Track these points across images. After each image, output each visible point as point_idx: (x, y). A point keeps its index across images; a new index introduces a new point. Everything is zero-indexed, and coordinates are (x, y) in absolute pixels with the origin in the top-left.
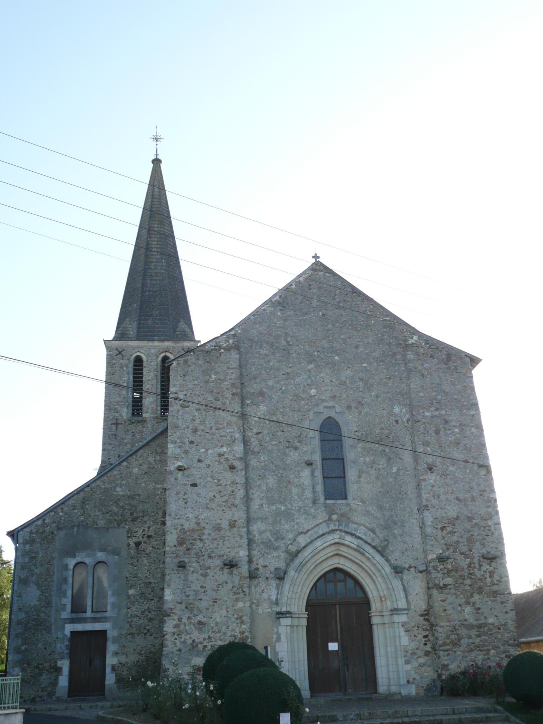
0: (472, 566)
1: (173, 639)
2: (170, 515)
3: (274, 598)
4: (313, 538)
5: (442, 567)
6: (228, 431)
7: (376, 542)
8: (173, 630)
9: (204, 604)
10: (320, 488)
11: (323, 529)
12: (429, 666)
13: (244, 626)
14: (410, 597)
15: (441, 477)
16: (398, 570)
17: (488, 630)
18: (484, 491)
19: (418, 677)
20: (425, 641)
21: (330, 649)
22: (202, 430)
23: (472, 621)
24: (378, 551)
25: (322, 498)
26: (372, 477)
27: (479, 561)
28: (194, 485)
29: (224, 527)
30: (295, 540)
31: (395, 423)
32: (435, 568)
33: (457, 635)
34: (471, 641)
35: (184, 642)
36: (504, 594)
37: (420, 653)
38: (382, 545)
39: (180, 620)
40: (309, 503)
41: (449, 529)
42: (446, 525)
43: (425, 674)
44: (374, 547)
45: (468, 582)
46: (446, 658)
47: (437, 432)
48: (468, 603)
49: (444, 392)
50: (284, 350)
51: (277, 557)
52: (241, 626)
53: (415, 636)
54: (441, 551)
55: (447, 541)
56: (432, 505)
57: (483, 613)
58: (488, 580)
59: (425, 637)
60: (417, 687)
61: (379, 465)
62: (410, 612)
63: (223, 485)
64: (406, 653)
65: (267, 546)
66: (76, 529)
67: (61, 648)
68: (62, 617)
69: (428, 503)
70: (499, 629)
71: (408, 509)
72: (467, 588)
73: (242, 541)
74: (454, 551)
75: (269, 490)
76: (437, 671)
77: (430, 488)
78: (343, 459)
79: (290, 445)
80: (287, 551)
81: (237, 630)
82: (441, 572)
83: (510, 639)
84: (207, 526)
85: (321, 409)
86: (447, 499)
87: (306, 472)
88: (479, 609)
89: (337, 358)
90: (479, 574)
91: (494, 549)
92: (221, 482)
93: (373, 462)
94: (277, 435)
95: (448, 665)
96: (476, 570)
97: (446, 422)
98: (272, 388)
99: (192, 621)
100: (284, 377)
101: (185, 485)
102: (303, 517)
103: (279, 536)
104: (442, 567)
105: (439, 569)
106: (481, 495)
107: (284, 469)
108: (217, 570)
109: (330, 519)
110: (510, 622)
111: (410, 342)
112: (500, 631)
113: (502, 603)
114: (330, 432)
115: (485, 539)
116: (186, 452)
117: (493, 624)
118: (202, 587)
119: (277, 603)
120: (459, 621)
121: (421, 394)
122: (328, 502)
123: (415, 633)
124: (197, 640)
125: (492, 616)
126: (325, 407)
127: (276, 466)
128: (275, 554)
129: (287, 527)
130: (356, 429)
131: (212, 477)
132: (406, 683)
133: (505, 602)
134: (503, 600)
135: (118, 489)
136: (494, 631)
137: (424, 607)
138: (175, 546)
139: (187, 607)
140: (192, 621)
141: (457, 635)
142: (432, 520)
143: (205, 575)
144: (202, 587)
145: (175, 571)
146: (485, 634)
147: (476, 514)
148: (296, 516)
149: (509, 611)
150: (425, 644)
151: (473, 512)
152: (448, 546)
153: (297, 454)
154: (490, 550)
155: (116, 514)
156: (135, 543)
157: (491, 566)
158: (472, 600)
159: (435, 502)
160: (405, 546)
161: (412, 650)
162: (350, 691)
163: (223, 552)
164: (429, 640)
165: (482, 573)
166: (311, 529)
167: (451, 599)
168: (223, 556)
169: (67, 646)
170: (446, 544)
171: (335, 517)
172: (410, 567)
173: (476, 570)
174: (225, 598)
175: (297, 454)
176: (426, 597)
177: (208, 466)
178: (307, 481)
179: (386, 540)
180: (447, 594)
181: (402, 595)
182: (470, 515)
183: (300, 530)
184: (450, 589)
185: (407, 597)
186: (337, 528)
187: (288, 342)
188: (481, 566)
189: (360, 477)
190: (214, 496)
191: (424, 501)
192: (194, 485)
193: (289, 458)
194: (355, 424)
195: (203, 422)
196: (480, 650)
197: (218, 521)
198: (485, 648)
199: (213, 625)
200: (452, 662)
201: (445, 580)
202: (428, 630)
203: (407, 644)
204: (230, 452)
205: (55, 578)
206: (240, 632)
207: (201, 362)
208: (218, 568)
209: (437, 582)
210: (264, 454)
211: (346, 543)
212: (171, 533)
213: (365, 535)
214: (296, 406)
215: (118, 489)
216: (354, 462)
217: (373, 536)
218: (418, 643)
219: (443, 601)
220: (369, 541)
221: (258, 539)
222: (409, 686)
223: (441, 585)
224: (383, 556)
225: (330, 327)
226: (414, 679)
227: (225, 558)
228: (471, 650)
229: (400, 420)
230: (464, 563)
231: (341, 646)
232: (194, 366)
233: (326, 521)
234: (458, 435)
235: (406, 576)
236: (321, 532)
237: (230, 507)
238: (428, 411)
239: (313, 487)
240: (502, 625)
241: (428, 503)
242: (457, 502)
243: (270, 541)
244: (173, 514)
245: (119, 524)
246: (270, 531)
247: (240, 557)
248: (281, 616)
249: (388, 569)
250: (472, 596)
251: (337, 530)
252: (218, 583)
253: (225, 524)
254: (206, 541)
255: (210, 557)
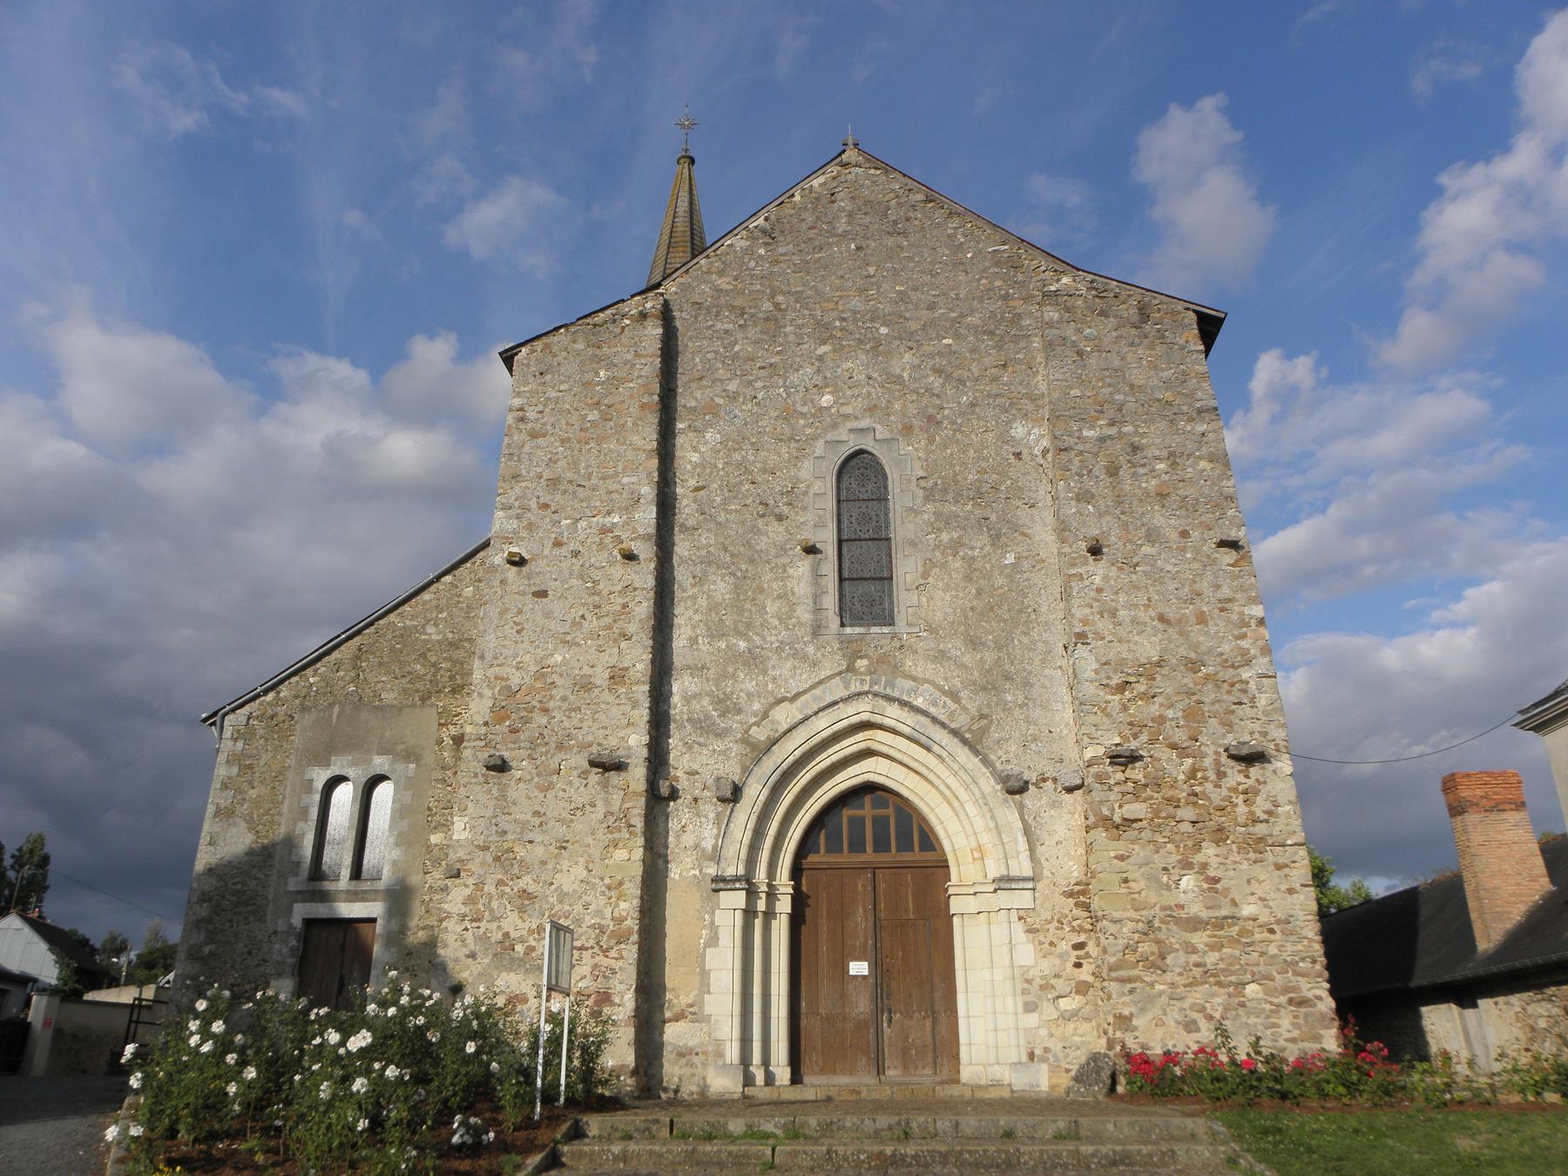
0: (1199, 775)
1: (459, 929)
2: (482, 657)
3: (708, 844)
4: (810, 712)
5: (1120, 776)
6: (626, 480)
7: (961, 721)
8: (464, 909)
9: (539, 852)
10: (830, 601)
11: (836, 690)
12: (1088, 1020)
13: (623, 905)
14: (1039, 850)
15: (1120, 569)
16: (1016, 788)
17: (1241, 934)
18: (1230, 600)
19: (1056, 1047)
20: (1078, 957)
21: (852, 972)
22: (570, 482)
23: (1196, 909)
24: (964, 741)
25: (834, 622)
26: (954, 575)
27: (1217, 763)
28: (542, 594)
29: (598, 683)
30: (765, 715)
31: (1012, 460)
32: (1101, 779)
33: (1158, 942)
34: (1194, 958)
35: (484, 939)
36: (1283, 845)
37: (1061, 986)
38: (975, 727)
39: (479, 886)
40: (804, 633)
41: (1142, 688)
42: (1132, 679)
43: (1076, 1038)
44: (955, 733)
45: (1187, 813)
46: (1127, 999)
47: (1113, 471)
48: (1187, 865)
49: (1132, 386)
50: (767, 319)
51: (723, 753)
52: (617, 905)
53: (1052, 944)
54: (1117, 740)
55: (1133, 716)
56: (1097, 633)
57: (1227, 890)
58: (1242, 809)
59: (1079, 946)
60: (1054, 1070)
61: (972, 548)
62: (1039, 886)
63: (605, 592)
64: (1026, 986)
65: (702, 728)
66: (336, 709)
67: (280, 951)
68: (291, 888)
69: (1087, 629)
70: (1272, 931)
71: (1041, 646)
72: (1186, 827)
73: (636, 712)
74: (1152, 741)
75: (713, 607)
76: (1105, 1033)
77: (1093, 594)
78: (888, 539)
79: (767, 510)
80: (746, 740)
81: (608, 912)
82: (1116, 789)
83: (1303, 959)
84: (560, 682)
85: (842, 434)
86: (1134, 621)
87: (804, 566)
88: (1216, 880)
89: (884, 330)
90: (1217, 796)
91: (1256, 735)
92: (601, 587)
93: (956, 546)
94: (739, 492)
95: (1130, 1018)
96: (1209, 786)
97: (1135, 449)
98: (733, 397)
99: (508, 890)
100: (762, 373)
101: (522, 594)
102: (789, 664)
103: (727, 707)
104: (1120, 776)
105: (1112, 782)
106: (1222, 610)
107: (751, 561)
108: (574, 778)
109: (850, 669)
110: (1301, 915)
111: (1052, 288)
112: (1272, 937)
113: (1278, 867)
114: (859, 475)
115: (1233, 712)
116: (530, 527)
117: (1255, 920)
118: (536, 814)
119: (716, 856)
120: (1164, 909)
121: (1076, 392)
122: (848, 630)
123: (1051, 937)
124: (513, 934)
125: (1252, 899)
126: (850, 430)
127: (732, 555)
128: (718, 745)
129: (750, 686)
130: (921, 473)
131: (581, 577)
132: (1024, 1058)
133: (1287, 866)
134: (1281, 861)
135: (430, 629)
136: (1258, 936)
137: (1075, 874)
138: (486, 724)
139: (497, 859)
140: (508, 890)
141: (1158, 942)
142: (1095, 666)
143: (546, 789)
144: (536, 814)
145: (481, 779)
146: (1233, 942)
147: (1210, 651)
148: (772, 663)
149: (1299, 888)
150: (1078, 965)
151: (1204, 648)
152: (1136, 727)
153: (781, 529)
154: (1247, 738)
155: (420, 678)
156: (453, 738)
157: (1247, 777)
158: (1199, 858)
159: (1103, 625)
160: (1033, 730)
161: (1044, 977)
162: (891, 1073)
163: (590, 738)
164: (1088, 956)
165: (1225, 792)
166: (805, 692)
167: (1140, 852)
168: (590, 745)
169: (292, 949)
170: (1130, 724)
171: (861, 664)
172: (1044, 780)
173: (1209, 786)
174: (589, 840)
175: (781, 529)
176: (1081, 851)
177: (576, 554)
178: (807, 585)
179: (982, 717)
180: (1133, 842)
181: (1022, 844)
182: (1193, 655)
183: (782, 693)
184: (1141, 830)
185: (1032, 850)
186: (866, 688)
187: (777, 306)
188: (1221, 775)
189: (925, 575)
190: (583, 617)
191: (1076, 622)
192: (542, 594)
193: (764, 539)
194: (919, 464)
195: (573, 465)
196: (1219, 984)
197: (587, 670)
198: (1233, 978)
199: (553, 900)
200: (1142, 1010)
201: (1126, 807)
202: (1086, 931)
203: (1031, 962)
204: (626, 523)
205: (285, 808)
206: (613, 919)
207: (580, 346)
208: (575, 773)
209: (1106, 812)
210: (709, 530)
211: (888, 722)
212: (480, 695)
213: (935, 704)
214: (788, 431)
215: (430, 629)
216: (913, 544)
217: (952, 705)
218: (1057, 961)
219: (1122, 858)
220: (942, 717)
221: (681, 712)
222: (1035, 1066)
223: (1117, 819)
224: (976, 752)
225: (872, 270)
226: (1047, 1050)
227: (595, 749)
228: (1193, 983)
229: (1025, 451)
230: (1178, 769)
231: (876, 967)
232: (564, 354)
233: (840, 673)
234: (1165, 477)
235: (1031, 799)
236: (829, 699)
237: (615, 640)
238: (1092, 428)
239: (816, 598)
240: (1278, 922)
241: (1087, 629)
242: (1160, 626)
243: (708, 717)
244: (489, 657)
245: (423, 699)
246: (710, 694)
247: (629, 748)
248: (721, 885)
249: (989, 784)
250: (1197, 847)
251: (866, 693)
252: (573, 805)
253: (601, 677)
254: (555, 713)
255: (560, 747)
